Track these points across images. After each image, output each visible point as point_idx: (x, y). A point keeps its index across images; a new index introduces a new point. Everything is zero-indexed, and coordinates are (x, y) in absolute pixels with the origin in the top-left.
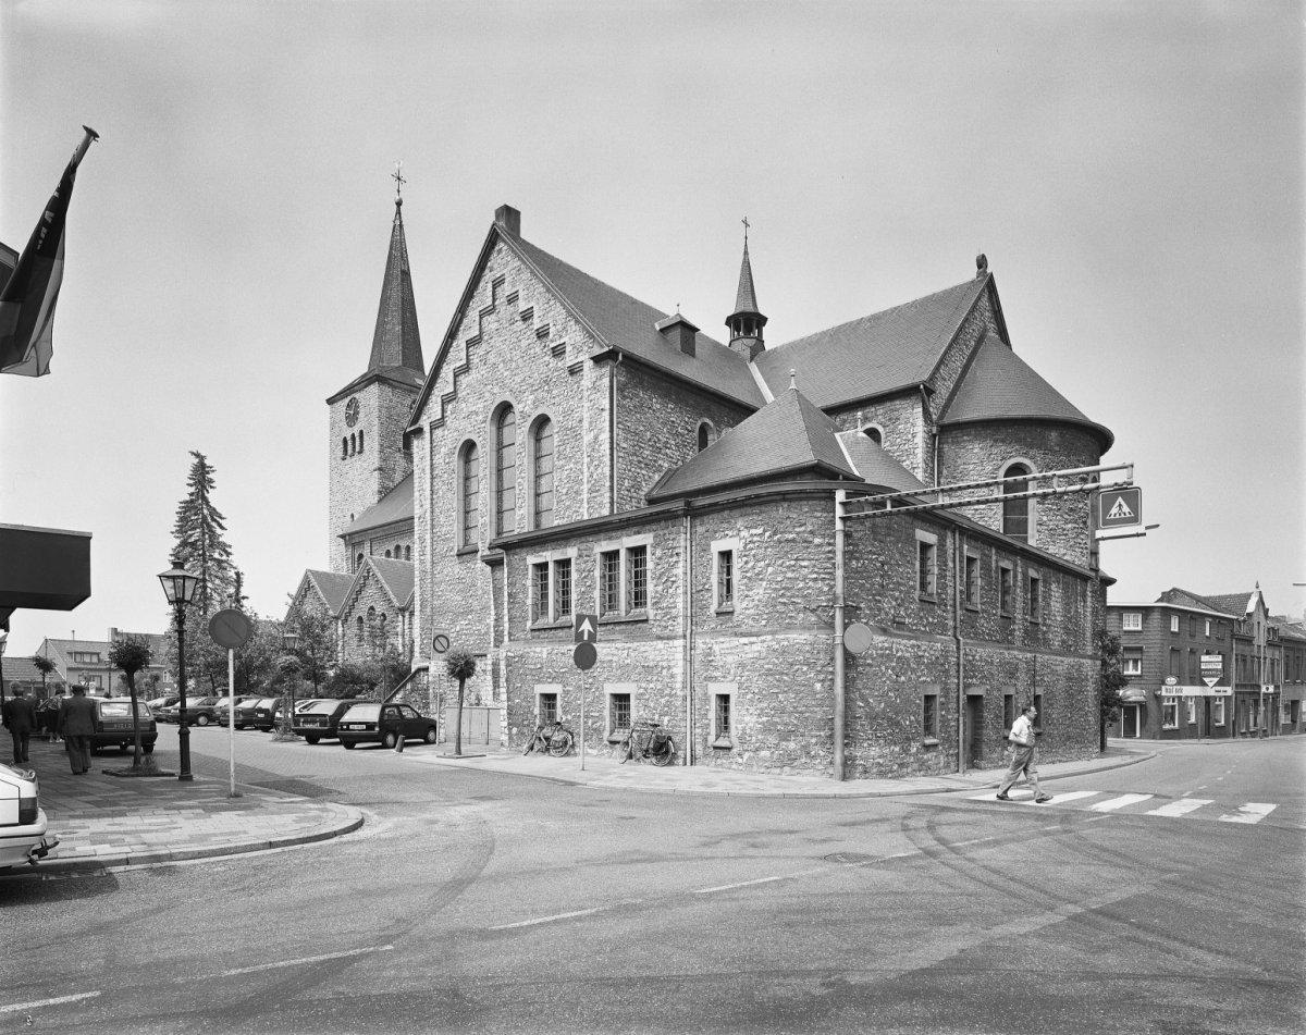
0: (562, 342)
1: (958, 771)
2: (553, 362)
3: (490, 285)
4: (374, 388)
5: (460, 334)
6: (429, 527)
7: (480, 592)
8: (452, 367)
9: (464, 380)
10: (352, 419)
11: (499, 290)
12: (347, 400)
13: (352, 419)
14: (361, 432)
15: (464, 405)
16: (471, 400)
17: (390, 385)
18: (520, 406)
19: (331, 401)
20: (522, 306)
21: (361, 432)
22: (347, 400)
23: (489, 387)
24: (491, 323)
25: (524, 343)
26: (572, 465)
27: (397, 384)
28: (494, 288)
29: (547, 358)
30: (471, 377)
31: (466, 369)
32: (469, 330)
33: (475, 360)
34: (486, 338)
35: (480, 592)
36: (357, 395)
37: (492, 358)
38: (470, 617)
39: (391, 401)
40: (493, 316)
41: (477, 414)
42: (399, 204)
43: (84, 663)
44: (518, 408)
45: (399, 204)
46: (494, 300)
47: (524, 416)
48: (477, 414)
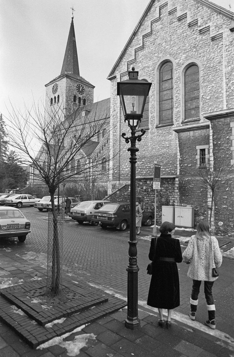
0: (207, 26)
1: (136, 259)
2: (199, 37)
3: (158, 9)
4: (65, 80)
5: (139, 33)
6: (119, 120)
7: (150, 149)
8: (134, 48)
9: (140, 54)
10: (55, 90)
11: (163, 10)
12: (53, 85)
13: (55, 90)
14: (59, 96)
15: (140, 64)
16: (144, 62)
17: (70, 79)
18: (177, 61)
19: (46, 86)
20: (179, 14)
21: (59, 96)
22: (53, 85)
23: (156, 55)
24: (157, 26)
25: (179, 31)
26: (213, 85)
27: (73, 79)
28: (160, 10)
29: (195, 36)
30: (144, 52)
31: (143, 48)
32: (146, 29)
33: (148, 43)
34: (154, 33)
35: (150, 149)
36: (57, 83)
37: (158, 41)
38: (143, 160)
39: (70, 84)
40: (159, 22)
41: (148, 67)
42: (73, 18)
43: (205, 12)
44: (175, 62)
45: (73, 18)
46: (160, 15)
47: (179, 65)
48: (148, 67)
